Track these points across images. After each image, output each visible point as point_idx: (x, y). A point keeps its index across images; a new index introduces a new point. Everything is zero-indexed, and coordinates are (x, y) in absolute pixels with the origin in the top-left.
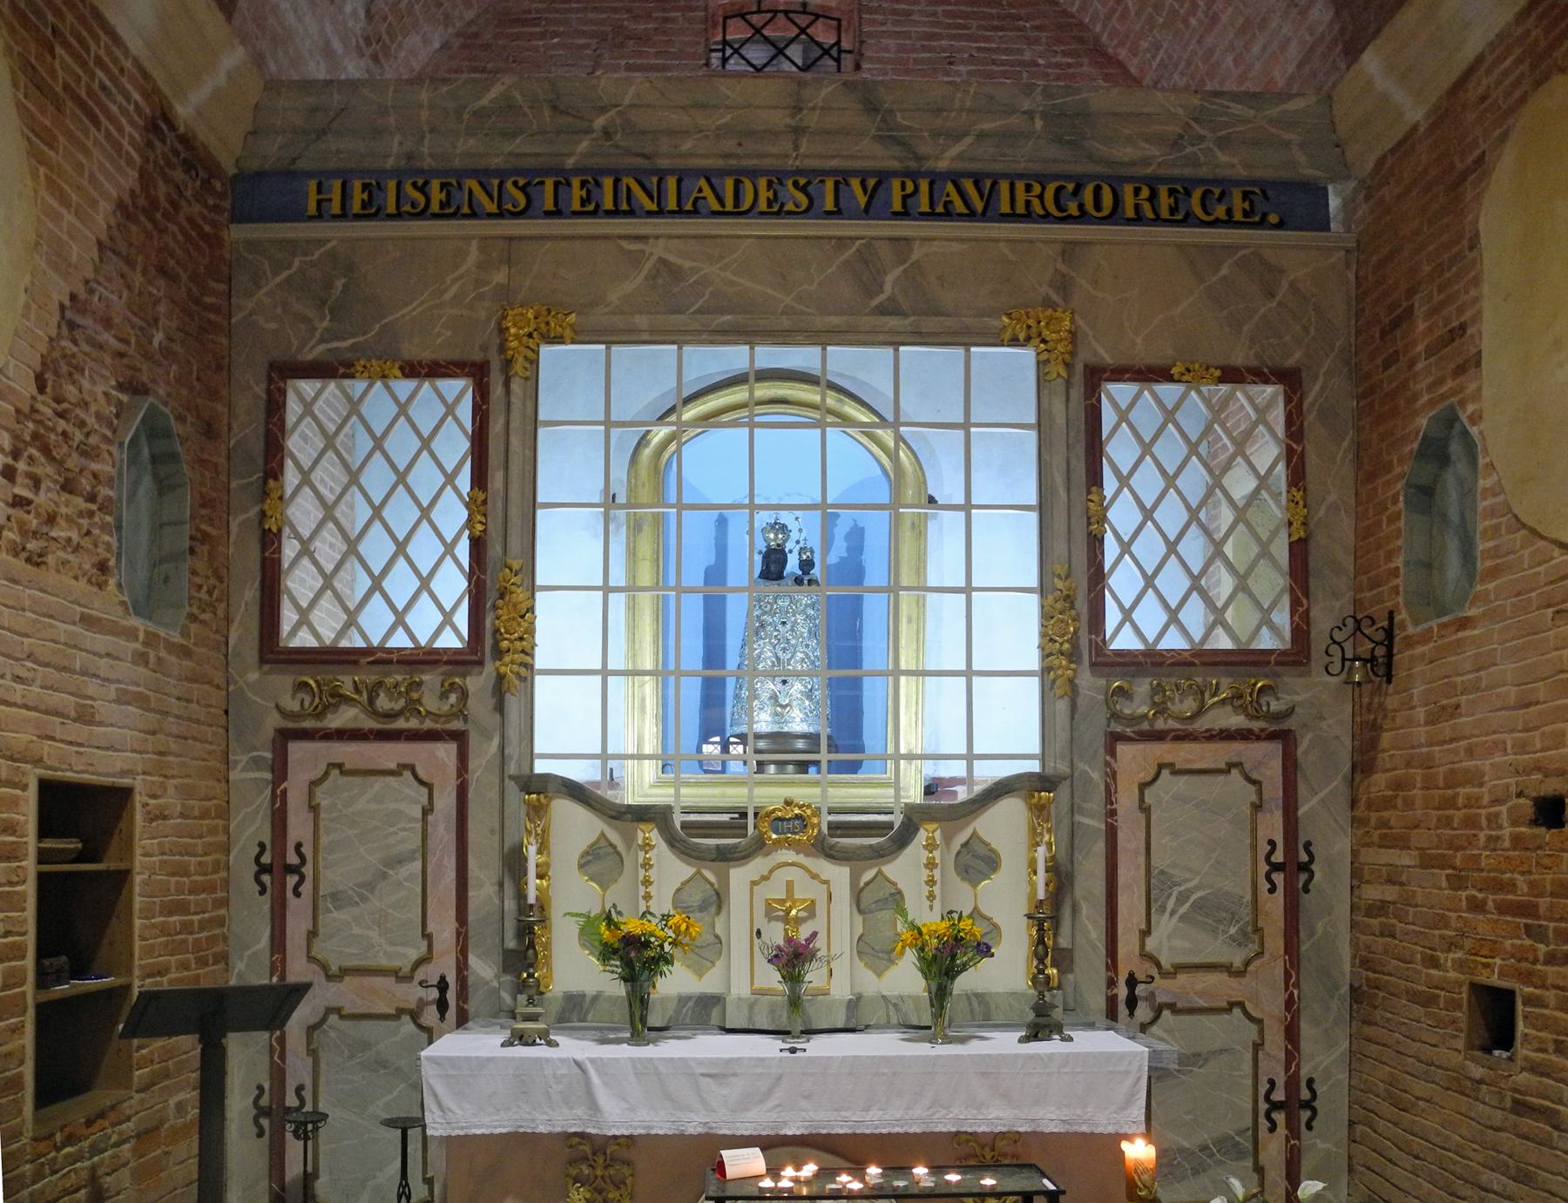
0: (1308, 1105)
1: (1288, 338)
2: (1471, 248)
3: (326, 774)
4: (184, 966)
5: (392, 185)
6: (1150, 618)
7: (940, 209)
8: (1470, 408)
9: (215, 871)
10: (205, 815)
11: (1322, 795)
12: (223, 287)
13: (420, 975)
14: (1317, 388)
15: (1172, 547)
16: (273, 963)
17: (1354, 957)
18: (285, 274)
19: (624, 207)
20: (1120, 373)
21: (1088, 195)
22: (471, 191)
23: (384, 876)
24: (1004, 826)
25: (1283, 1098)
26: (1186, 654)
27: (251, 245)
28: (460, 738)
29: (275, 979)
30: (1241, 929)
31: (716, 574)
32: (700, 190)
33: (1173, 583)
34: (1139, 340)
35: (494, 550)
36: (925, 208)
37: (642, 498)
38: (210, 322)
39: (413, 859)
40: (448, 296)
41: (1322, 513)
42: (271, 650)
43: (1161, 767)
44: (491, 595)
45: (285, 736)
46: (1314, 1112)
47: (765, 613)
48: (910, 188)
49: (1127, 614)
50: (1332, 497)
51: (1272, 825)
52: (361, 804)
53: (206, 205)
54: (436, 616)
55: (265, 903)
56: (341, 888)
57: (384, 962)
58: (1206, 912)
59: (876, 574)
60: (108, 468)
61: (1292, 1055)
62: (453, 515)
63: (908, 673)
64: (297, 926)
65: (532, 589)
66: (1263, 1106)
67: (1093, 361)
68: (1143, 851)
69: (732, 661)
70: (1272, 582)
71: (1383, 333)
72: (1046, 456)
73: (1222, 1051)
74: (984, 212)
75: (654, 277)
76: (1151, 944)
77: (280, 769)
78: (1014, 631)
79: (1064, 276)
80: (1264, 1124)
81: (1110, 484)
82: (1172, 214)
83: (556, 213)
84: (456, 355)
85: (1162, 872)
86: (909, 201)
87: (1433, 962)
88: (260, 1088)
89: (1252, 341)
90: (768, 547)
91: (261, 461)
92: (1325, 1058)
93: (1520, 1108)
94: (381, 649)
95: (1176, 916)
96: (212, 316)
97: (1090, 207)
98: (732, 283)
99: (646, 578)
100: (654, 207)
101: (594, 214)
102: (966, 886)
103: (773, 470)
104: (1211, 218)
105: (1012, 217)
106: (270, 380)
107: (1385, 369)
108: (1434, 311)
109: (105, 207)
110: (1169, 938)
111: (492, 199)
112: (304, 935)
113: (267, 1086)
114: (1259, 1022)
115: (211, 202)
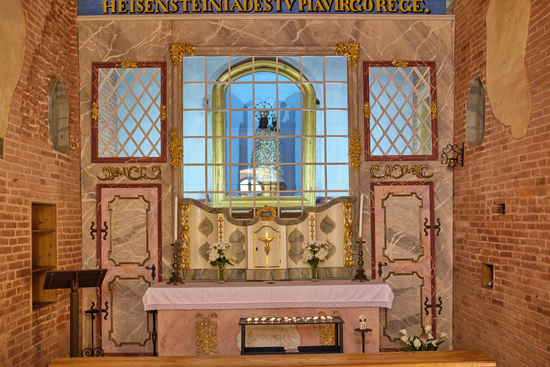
1: (431, 51)
2: (484, 26)
4: (70, 262)
6: (385, 145)
7: (315, 9)
8: (484, 79)
9: (78, 231)
10: (75, 213)
11: (443, 203)
12: (75, 37)
13: (146, 265)
14: (441, 68)
15: (392, 122)
16: (97, 262)
17: (454, 257)
19: (210, 10)
20: (164, 72)
22: (158, 4)
23: (134, 233)
24: (335, 214)
25: (437, 308)
27: (84, 22)
28: (159, 186)
29: (98, 267)
32: (235, 4)
33: (393, 133)
34: (381, 53)
35: (169, 125)
36: (310, 9)
37: (217, 101)
38: (72, 49)
39: (144, 227)
40: (152, 40)
41: (442, 110)
42: (95, 158)
43: (389, 194)
45: (99, 187)
46: (441, 308)
47: (261, 140)
49: (377, 144)
50: (446, 104)
51: (426, 213)
52: (126, 209)
53: (69, 10)
54: (151, 148)
55: (94, 243)
56: (119, 236)
57: (134, 261)
58: (405, 242)
60: (46, 103)
61: (433, 290)
62: (155, 113)
64: (105, 250)
65: (182, 137)
66: (424, 306)
67: (366, 60)
68: (383, 222)
71: (462, 50)
72: (350, 92)
73: (410, 288)
74: (329, 11)
75: (221, 34)
76: (386, 252)
77: (99, 198)
78: (340, 149)
80: (424, 312)
81: (372, 100)
82: (392, 9)
83: (187, 12)
84: (154, 60)
85: (390, 229)
86: (305, 7)
87: (473, 257)
88: (93, 303)
89: (419, 52)
90: (261, 117)
91: (90, 96)
92: (445, 290)
93: (494, 302)
94: (132, 158)
95: (395, 244)
96: (73, 47)
98: (247, 35)
99: (219, 133)
101: (200, 12)
102: (324, 234)
103: (265, 91)
105: (339, 12)
106: (93, 69)
107: (462, 62)
108: (474, 45)
109: (43, 19)
110: (393, 250)
112: (107, 252)
113: (95, 302)
114: (422, 278)
115: (71, 8)
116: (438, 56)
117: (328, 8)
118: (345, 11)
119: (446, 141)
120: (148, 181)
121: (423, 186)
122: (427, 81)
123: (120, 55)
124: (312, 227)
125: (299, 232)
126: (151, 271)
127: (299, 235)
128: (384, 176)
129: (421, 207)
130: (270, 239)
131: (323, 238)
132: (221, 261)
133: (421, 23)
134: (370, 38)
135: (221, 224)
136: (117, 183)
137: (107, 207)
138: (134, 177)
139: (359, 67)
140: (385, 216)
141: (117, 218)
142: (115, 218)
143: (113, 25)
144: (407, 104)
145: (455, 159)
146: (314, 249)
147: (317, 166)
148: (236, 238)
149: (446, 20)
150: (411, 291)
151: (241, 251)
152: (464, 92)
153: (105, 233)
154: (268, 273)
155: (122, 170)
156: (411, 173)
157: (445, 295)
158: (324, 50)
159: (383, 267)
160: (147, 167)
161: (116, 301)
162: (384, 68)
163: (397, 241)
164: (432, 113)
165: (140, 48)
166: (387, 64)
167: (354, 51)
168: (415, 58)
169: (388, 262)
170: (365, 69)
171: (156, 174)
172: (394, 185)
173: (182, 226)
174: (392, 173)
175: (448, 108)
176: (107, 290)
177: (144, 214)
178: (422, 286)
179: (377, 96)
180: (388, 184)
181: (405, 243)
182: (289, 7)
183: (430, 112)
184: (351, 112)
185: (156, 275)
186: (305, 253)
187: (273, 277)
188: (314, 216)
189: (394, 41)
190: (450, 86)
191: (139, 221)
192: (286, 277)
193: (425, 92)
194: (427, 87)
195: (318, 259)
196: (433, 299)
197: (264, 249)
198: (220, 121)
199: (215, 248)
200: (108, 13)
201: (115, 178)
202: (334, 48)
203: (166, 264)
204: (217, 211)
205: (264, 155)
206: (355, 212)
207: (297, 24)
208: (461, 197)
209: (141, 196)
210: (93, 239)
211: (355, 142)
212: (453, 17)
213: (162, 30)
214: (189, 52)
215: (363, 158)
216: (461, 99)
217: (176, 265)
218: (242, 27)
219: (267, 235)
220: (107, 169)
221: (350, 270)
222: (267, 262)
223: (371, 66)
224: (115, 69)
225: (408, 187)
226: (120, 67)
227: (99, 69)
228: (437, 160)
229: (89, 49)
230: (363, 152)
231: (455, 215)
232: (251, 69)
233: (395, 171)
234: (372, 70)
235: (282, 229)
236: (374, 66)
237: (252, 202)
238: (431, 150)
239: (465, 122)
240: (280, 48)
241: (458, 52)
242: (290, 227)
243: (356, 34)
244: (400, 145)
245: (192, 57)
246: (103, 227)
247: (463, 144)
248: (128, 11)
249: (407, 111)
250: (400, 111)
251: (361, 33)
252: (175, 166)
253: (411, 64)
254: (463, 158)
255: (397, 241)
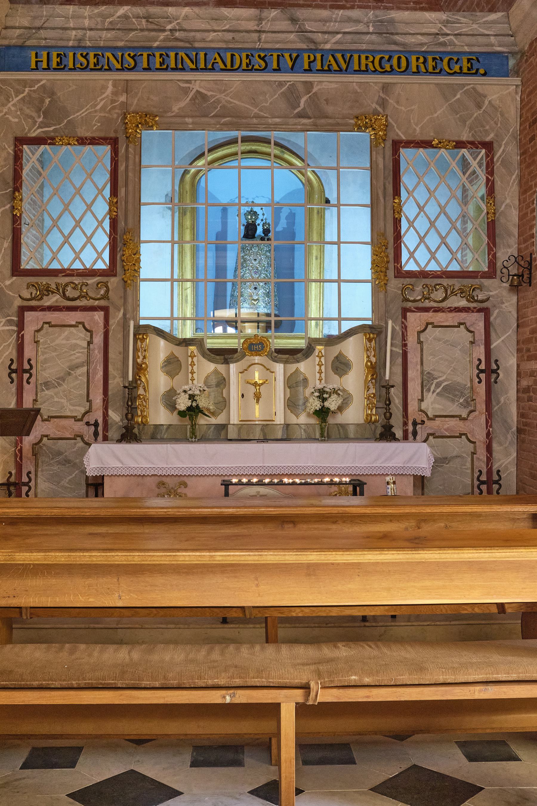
0: (496, 482)
1: (487, 127)
3: (42, 327)
5: (71, 54)
6: (422, 256)
11: (503, 338)
13: (86, 419)
14: (501, 150)
17: (518, 413)
18: (22, 96)
20: (115, 152)
21: (395, 61)
22: (108, 58)
23: (69, 374)
24: (353, 350)
25: (494, 485)
26: (439, 273)
28: (105, 310)
30: (465, 400)
31: (222, 235)
32: (215, 59)
33: (433, 241)
34: (418, 129)
35: (121, 224)
36: (319, 67)
37: (186, 199)
39: (83, 366)
40: (98, 107)
42: (16, 269)
43: (428, 324)
44: (120, 245)
45: (22, 310)
46: (500, 486)
47: (246, 255)
48: (312, 58)
49: (412, 254)
50: (508, 201)
51: (480, 352)
52: (57, 342)
54: (94, 253)
55: (13, 388)
57: (69, 414)
58: (450, 391)
59: (300, 236)
62: (102, 208)
63: (315, 281)
65: (139, 242)
66: (476, 483)
67: (396, 138)
68: (419, 363)
69: (230, 275)
70: (476, 236)
72: (374, 182)
74: (346, 70)
76: (424, 406)
77: (21, 325)
78: (359, 261)
79: (383, 99)
82: (434, 70)
83: (148, 69)
84: (102, 135)
85: (428, 373)
88: (10, 473)
89: (471, 129)
91: (11, 183)
94: (68, 269)
95: (435, 394)
97: (395, 66)
98: (231, 103)
100: (194, 67)
101: (166, 69)
102: (337, 377)
103: (252, 185)
104: (452, 72)
105: (359, 71)
106: (16, 146)
107: (530, 142)
110: (432, 403)
111: (118, 62)
112: (31, 401)
113: (13, 472)
114: (474, 443)
116: (496, 135)
117: (344, 66)
118: (367, 71)
119: (507, 251)
120: (91, 303)
121: (475, 314)
122: (482, 171)
123: (53, 128)
124: (320, 365)
125: (301, 373)
126: (93, 428)
127: (302, 377)
128: (420, 300)
129: (472, 343)
130: (261, 382)
131: (335, 382)
132: (193, 411)
133: (474, 88)
134: (403, 108)
135: (192, 361)
136: (47, 304)
137: (32, 338)
138: (71, 296)
139: (386, 148)
140: (422, 355)
141: (46, 353)
142: (44, 353)
143: (43, 86)
144: (453, 201)
145: (520, 276)
146: (322, 395)
147: (264, 629)
148: (213, 381)
149: (508, 85)
150: (458, 460)
151: (221, 399)
152: (533, 183)
153: (28, 375)
154: (258, 429)
155: (53, 286)
156: (459, 295)
157: (506, 468)
158: (338, 124)
159: (418, 427)
160: (89, 282)
161: (42, 471)
162: (421, 149)
163: (438, 390)
164: (488, 213)
165: (82, 117)
166: (426, 144)
167: (380, 126)
168: (465, 137)
169: (425, 419)
170: (396, 151)
171: (102, 292)
172: (435, 311)
173: (138, 363)
174: (432, 295)
175: (511, 207)
176: (30, 455)
177: (84, 348)
178: (473, 453)
179: (411, 188)
180: (426, 310)
181: (449, 393)
182: (290, 64)
183: (485, 211)
184: (375, 210)
185: (101, 432)
186: (311, 400)
187: (265, 435)
188: (323, 351)
189: (436, 112)
190: (514, 177)
191: (76, 358)
192: (283, 435)
193: (480, 190)
194: (482, 176)
195: (328, 409)
196: (489, 472)
197: (252, 395)
198: (189, 226)
199: (185, 391)
200: (37, 69)
201: (45, 297)
202: (352, 121)
203: (114, 418)
204: (186, 342)
205: (252, 276)
206: (380, 349)
207: (301, 88)
208: (527, 330)
209: (80, 323)
210: (12, 382)
211: (380, 250)
212: (517, 81)
213: (113, 93)
214: (150, 124)
215: (391, 273)
216: (528, 194)
217: (130, 416)
218: (225, 91)
219: (257, 377)
220: (33, 286)
221: (373, 427)
222: (257, 413)
223: (404, 147)
224: (47, 146)
225: (453, 314)
226: (54, 144)
227: (25, 146)
228: (495, 278)
229: (10, 118)
230: (391, 266)
231: (520, 355)
232: (236, 154)
233: (435, 292)
234: (405, 153)
235: (279, 368)
236: (408, 147)
237: (237, 341)
238: (487, 265)
239: (534, 225)
240: (278, 120)
241: (525, 129)
242: (288, 366)
243: (383, 103)
244: (444, 256)
245: (155, 131)
246: (26, 366)
247: (531, 254)
248: (65, 66)
249: (454, 210)
250: (443, 210)
251: (391, 101)
252: (129, 282)
253: (460, 145)
254: (530, 273)
255: (438, 390)
